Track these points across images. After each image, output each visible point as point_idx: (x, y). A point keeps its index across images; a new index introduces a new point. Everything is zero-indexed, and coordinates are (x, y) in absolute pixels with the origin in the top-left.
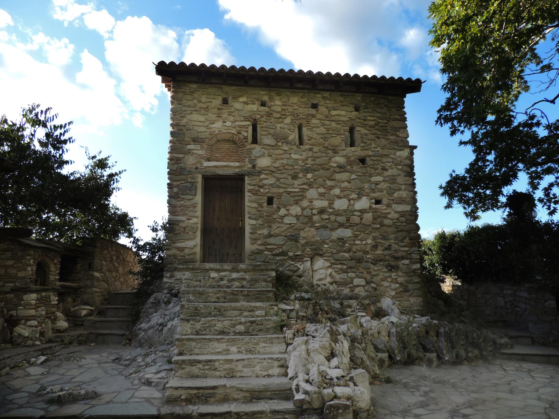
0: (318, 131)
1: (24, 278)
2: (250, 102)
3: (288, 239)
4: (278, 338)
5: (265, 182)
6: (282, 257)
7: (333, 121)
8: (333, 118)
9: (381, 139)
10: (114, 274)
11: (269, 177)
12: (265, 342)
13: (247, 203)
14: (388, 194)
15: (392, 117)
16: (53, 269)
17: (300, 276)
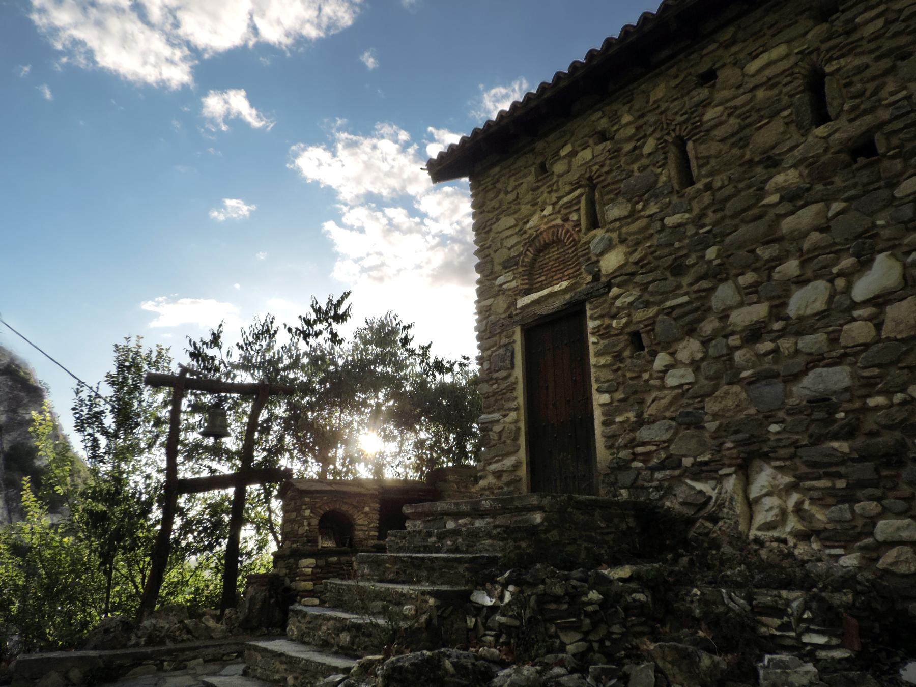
3: (680, 424)
5: (618, 303)
6: (668, 472)
13: (593, 360)
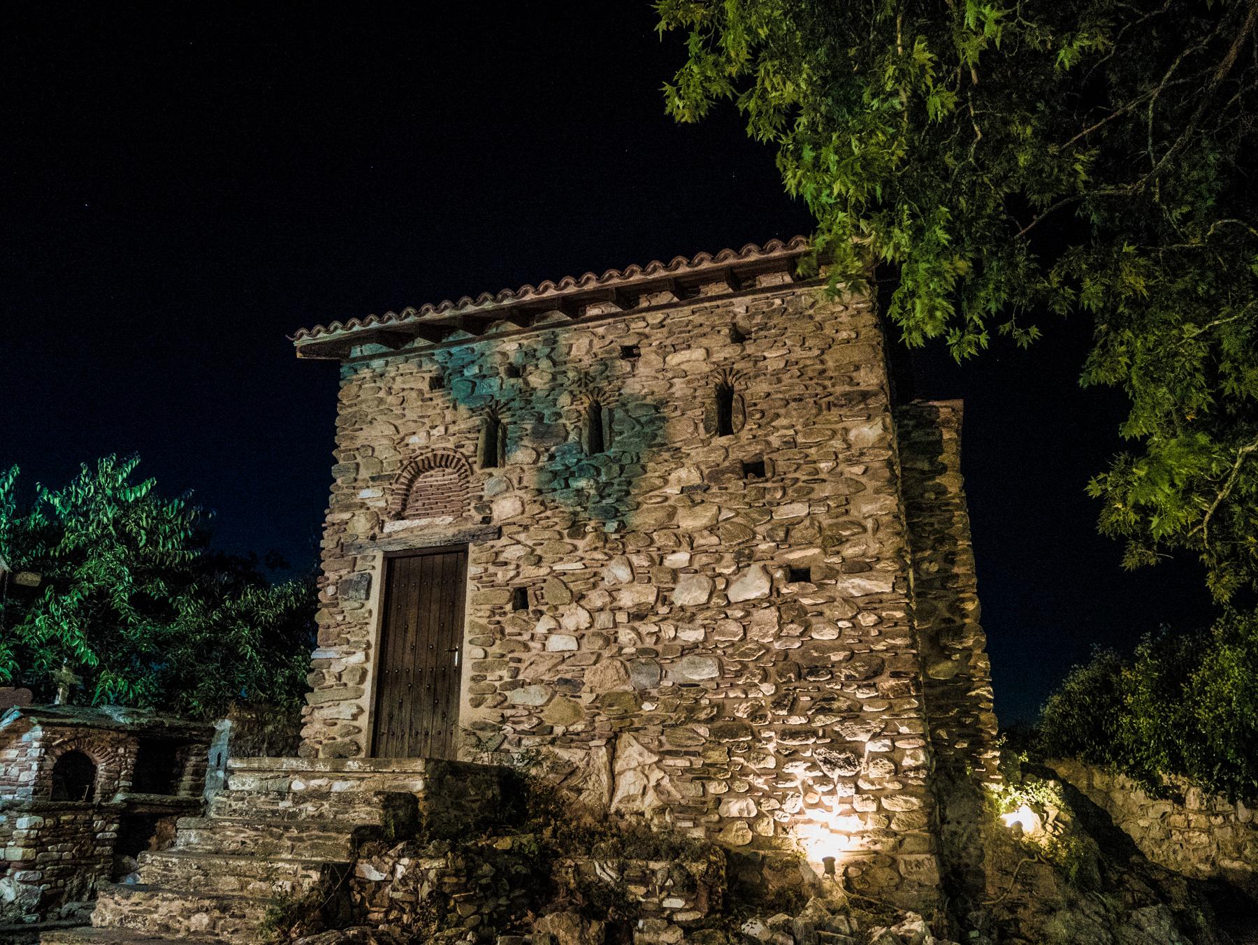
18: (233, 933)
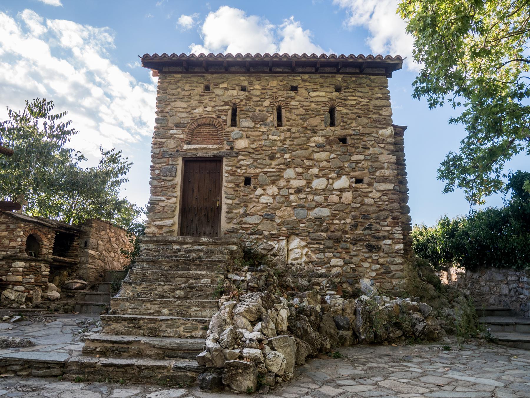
0: (297, 112)
1: (14, 248)
2: (230, 88)
3: (264, 218)
4: (210, 302)
5: (242, 163)
7: (312, 102)
8: (312, 100)
9: (363, 118)
10: (112, 254)
11: (247, 157)
12: (196, 306)
13: (224, 184)
14: (370, 172)
15: (374, 96)
16: (46, 242)
17: (275, 255)
18: (198, 297)
